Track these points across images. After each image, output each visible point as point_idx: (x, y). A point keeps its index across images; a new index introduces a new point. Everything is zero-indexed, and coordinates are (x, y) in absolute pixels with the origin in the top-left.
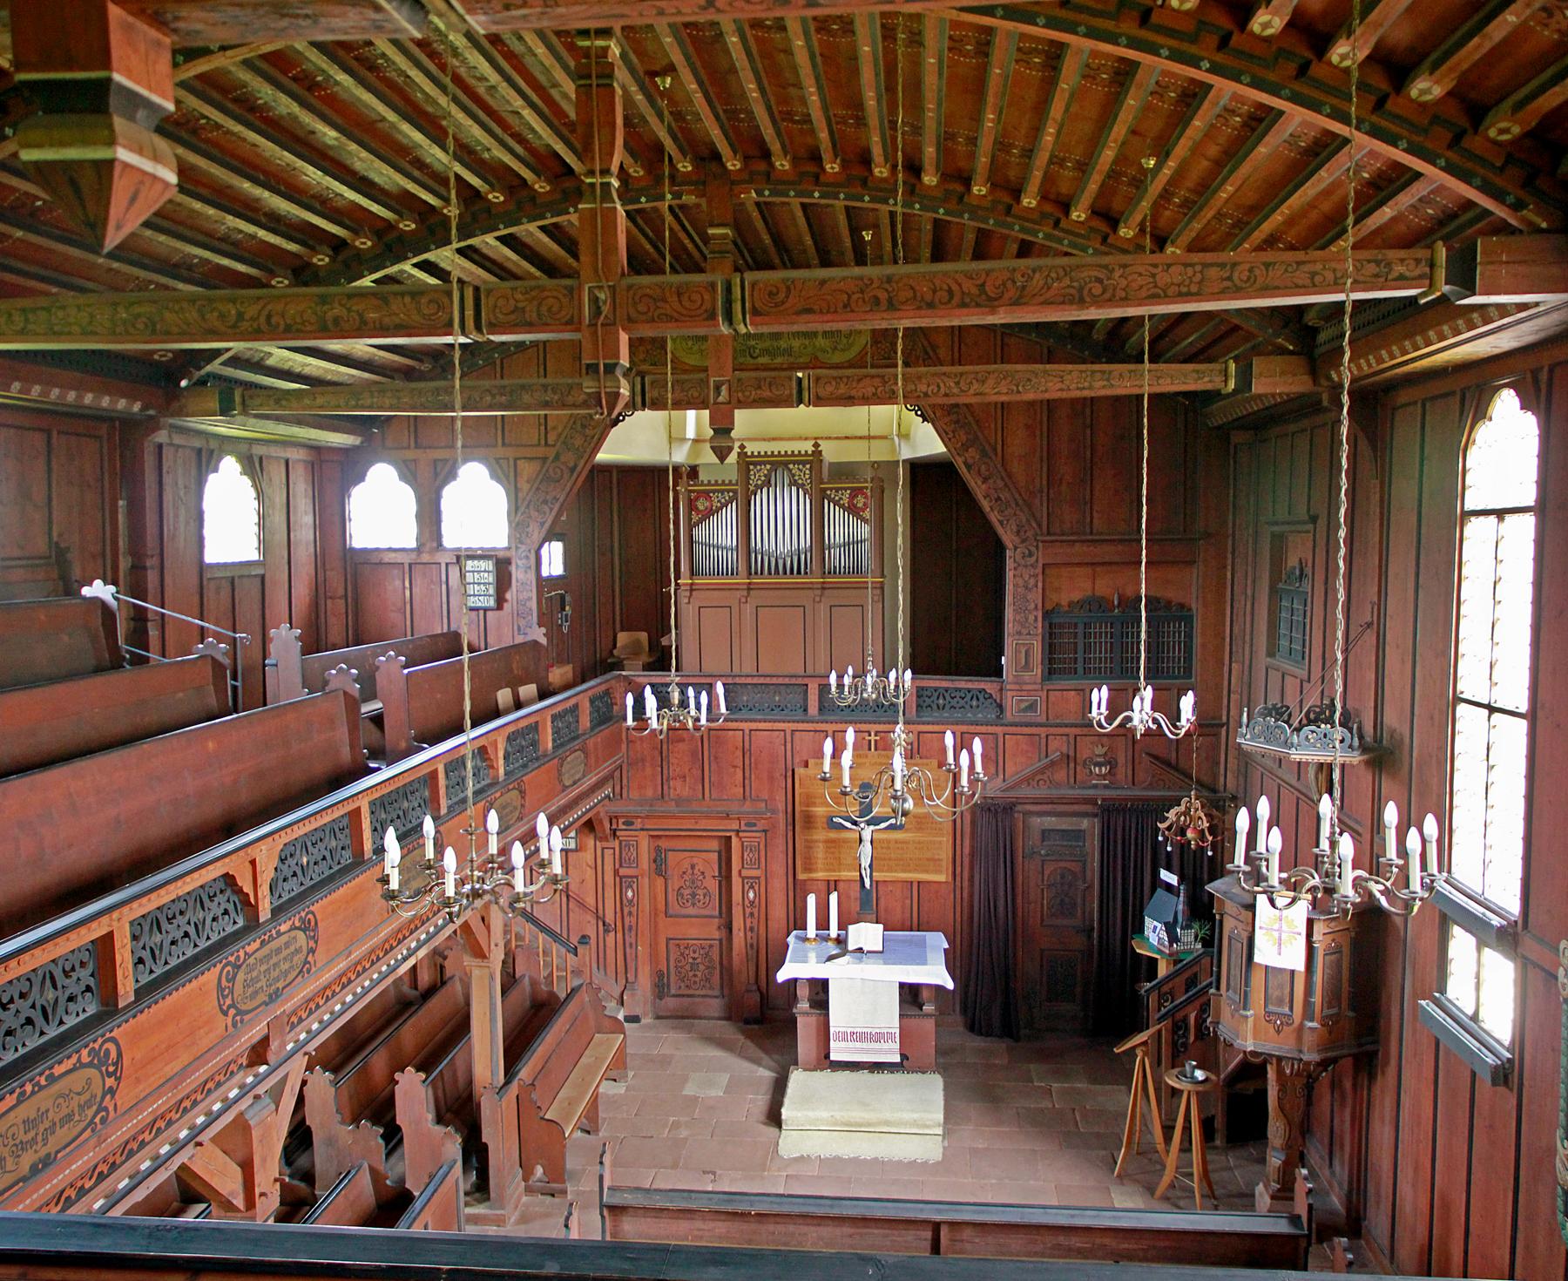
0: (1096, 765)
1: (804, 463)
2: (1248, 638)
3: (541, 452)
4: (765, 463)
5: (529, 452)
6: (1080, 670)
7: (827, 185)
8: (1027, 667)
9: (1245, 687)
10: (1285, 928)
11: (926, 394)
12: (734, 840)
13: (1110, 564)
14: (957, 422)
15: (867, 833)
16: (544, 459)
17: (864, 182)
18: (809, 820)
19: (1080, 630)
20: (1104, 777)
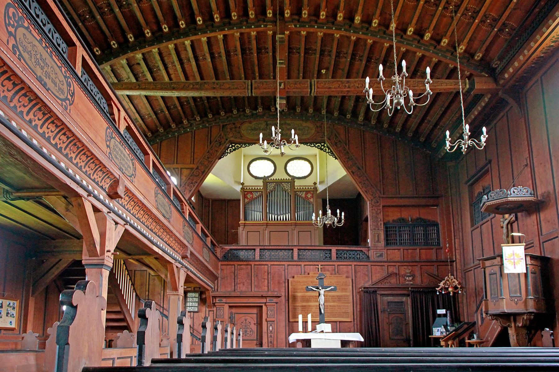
0: (407, 276)
1: (288, 183)
2: (460, 230)
3: (191, 166)
4: (273, 182)
5: (187, 166)
6: (398, 244)
7: (320, 24)
8: (379, 241)
9: (461, 247)
10: (516, 258)
11: (358, 87)
12: (264, 307)
13: (409, 206)
14: (349, 158)
15: (322, 292)
16: (192, 169)
17: (333, 23)
18: (295, 298)
19: (397, 229)
20: (411, 281)
